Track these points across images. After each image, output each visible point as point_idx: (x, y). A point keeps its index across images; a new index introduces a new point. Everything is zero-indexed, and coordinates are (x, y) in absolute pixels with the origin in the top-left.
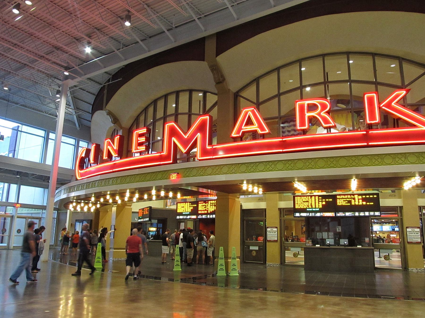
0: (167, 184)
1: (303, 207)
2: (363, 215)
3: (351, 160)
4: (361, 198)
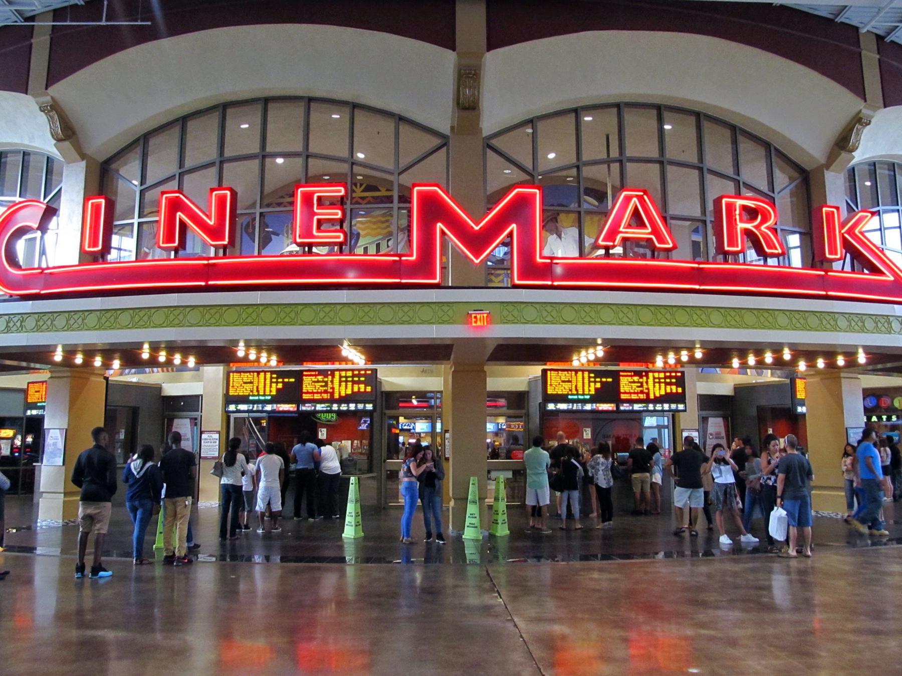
0: (361, 337)
1: (561, 393)
2: (345, 408)
3: (583, 312)
4: (663, 376)
